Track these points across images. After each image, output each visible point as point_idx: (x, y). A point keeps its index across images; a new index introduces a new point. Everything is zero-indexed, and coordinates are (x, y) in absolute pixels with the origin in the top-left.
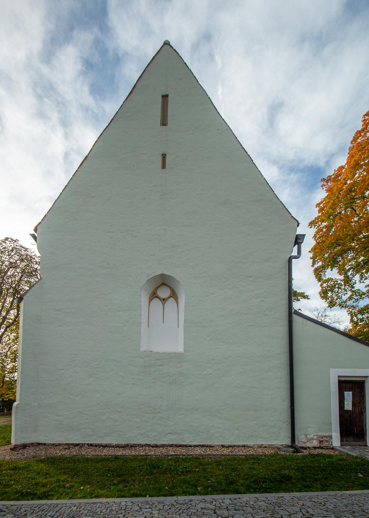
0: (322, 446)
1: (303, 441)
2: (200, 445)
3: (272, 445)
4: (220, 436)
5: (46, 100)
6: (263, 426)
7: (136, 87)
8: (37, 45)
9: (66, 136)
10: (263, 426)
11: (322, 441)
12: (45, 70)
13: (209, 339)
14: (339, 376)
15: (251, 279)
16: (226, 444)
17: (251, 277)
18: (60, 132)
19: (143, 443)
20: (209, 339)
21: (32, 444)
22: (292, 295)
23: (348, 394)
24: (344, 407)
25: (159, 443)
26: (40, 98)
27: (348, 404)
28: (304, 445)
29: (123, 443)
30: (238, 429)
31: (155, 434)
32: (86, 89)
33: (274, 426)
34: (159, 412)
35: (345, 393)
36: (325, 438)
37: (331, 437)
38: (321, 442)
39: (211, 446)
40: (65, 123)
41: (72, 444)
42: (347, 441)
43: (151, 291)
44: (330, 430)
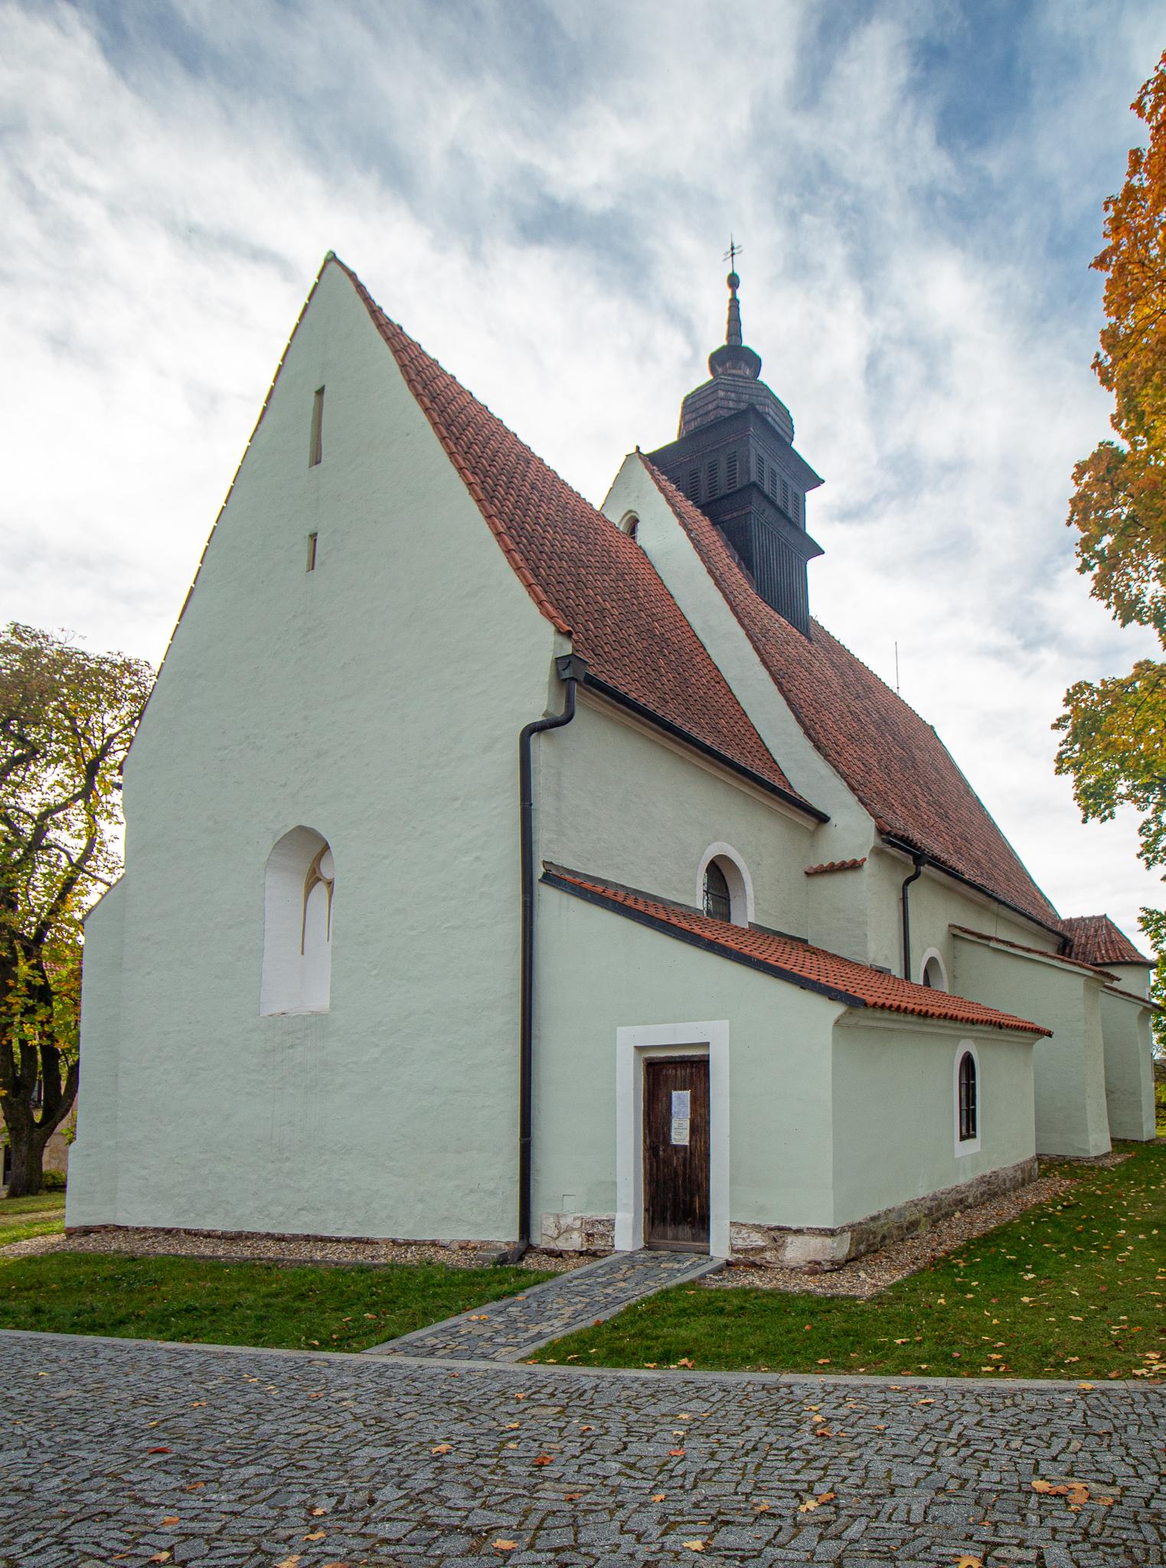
0: (593, 1248)
1: (550, 1233)
2: (354, 1239)
3: (489, 1243)
4: (389, 1217)
5: (807, 219)
6: (472, 1191)
7: (275, 394)
8: (779, 67)
9: (870, 304)
10: (472, 1191)
11: (592, 1235)
12: (805, 130)
13: (374, 972)
14: (639, 1049)
15: (457, 804)
16: (401, 1237)
17: (456, 799)
18: (851, 299)
19: (263, 1231)
20: (374, 972)
21: (105, 1227)
22: (103, 896)
23: (679, 1097)
24: (670, 1135)
25: (288, 1231)
26: (792, 219)
27: (680, 1127)
28: (552, 1246)
29: (234, 1229)
30: (421, 1200)
31: (281, 1209)
32: (925, 135)
33: (493, 1193)
34: (288, 1159)
35: (674, 1094)
36: (601, 1228)
37: (611, 1223)
38: (590, 1236)
39: (368, 1242)
40: (865, 266)
41: (163, 1229)
42: (676, 1238)
43: (306, 868)
44: (613, 1204)
